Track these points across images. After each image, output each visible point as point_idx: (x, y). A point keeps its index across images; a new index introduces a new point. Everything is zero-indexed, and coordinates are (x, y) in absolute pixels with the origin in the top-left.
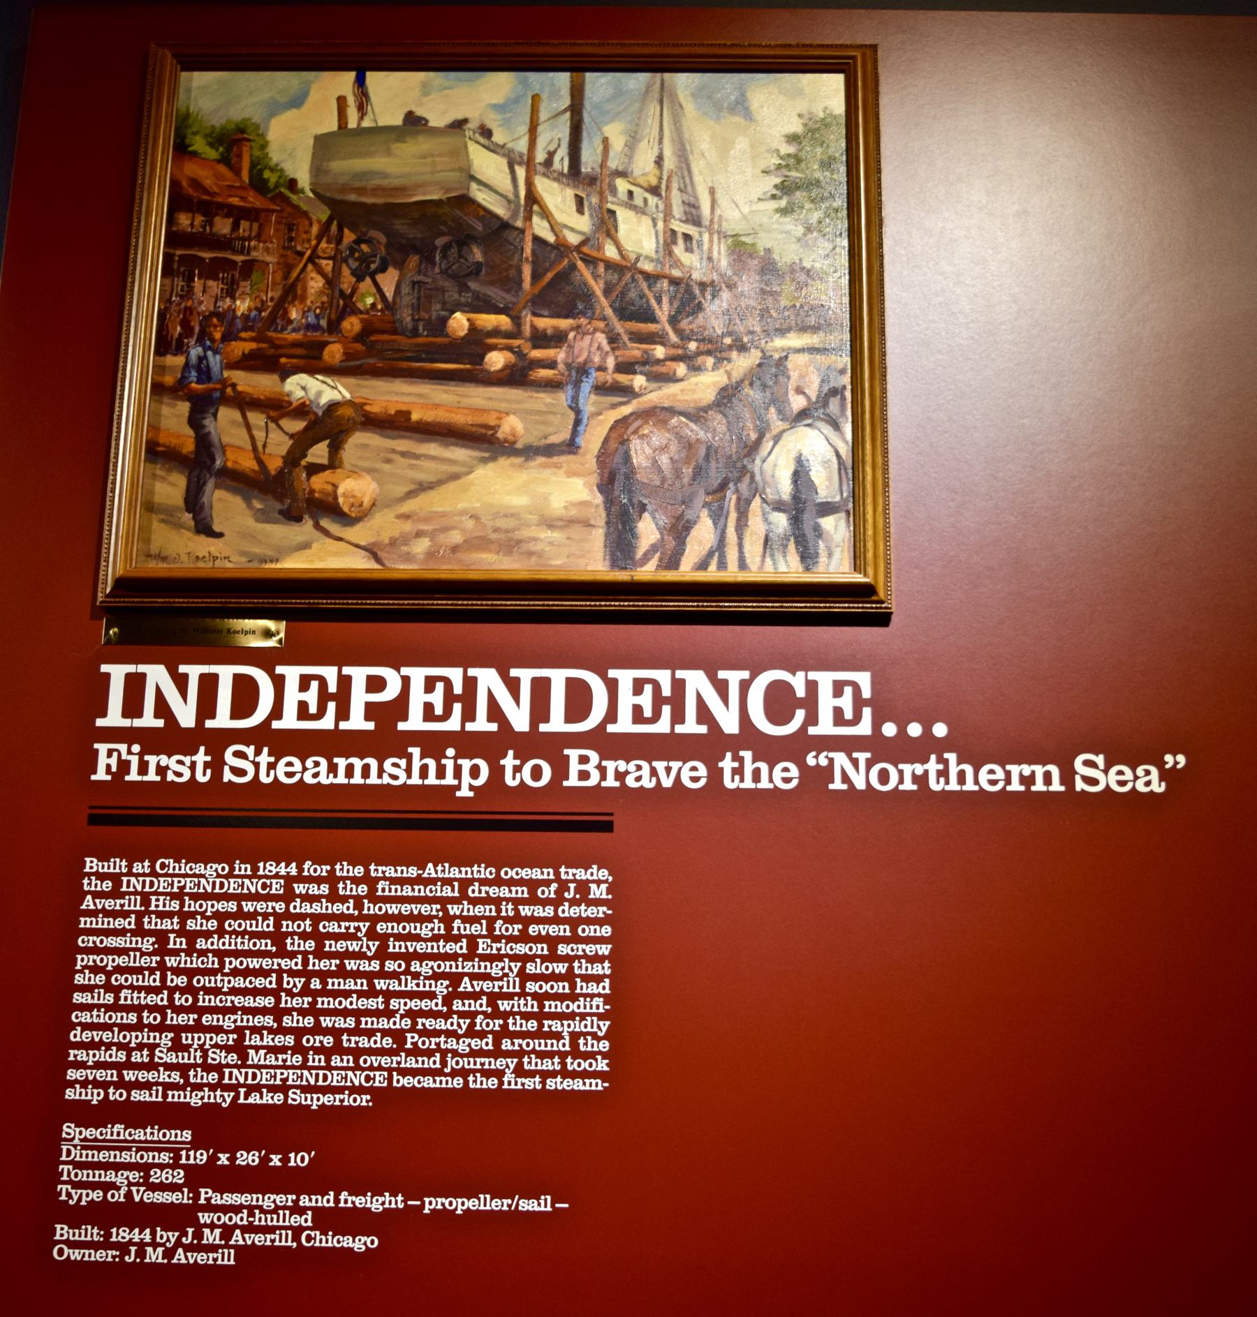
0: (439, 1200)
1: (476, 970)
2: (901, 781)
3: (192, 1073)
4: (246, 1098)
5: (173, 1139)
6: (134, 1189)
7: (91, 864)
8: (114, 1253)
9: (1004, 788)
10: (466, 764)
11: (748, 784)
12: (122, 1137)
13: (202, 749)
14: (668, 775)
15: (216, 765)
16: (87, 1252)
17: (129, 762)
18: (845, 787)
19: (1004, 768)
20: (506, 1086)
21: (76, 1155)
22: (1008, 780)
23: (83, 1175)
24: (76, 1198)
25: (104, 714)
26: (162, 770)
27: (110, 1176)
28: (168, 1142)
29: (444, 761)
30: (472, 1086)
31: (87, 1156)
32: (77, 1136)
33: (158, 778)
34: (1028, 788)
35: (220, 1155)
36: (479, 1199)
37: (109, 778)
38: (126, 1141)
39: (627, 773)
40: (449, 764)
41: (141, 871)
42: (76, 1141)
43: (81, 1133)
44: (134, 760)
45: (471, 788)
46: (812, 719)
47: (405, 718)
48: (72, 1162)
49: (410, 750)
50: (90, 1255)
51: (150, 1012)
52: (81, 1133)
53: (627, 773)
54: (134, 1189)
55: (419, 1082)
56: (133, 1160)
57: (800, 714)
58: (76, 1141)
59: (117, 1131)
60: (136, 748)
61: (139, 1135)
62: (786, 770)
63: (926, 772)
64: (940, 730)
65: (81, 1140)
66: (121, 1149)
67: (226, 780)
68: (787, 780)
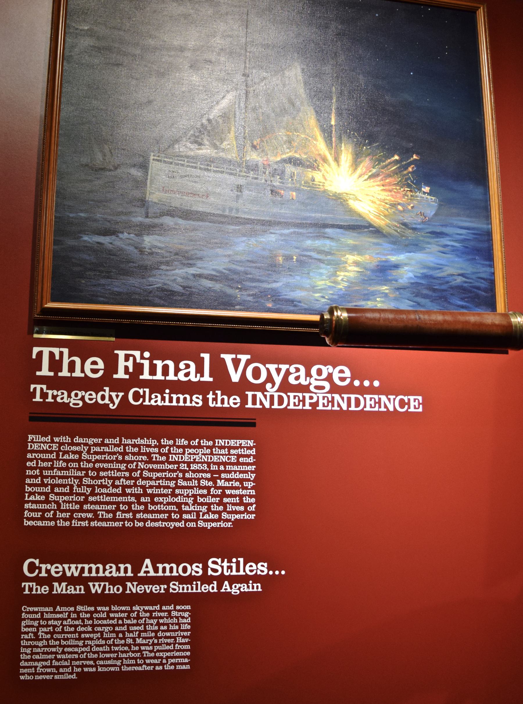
11: (219, 405)
14: (117, 398)
17: (143, 364)
18: (339, 409)
20: (73, 525)
25: (116, 373)
26: (81, 524)
29: (164, 395)
39: (57, 396)
41: (224, 453)
47: (117, 373)
53: (57, 396)
55: (36, 523)
62: (235, 399)
64: (376, 384)
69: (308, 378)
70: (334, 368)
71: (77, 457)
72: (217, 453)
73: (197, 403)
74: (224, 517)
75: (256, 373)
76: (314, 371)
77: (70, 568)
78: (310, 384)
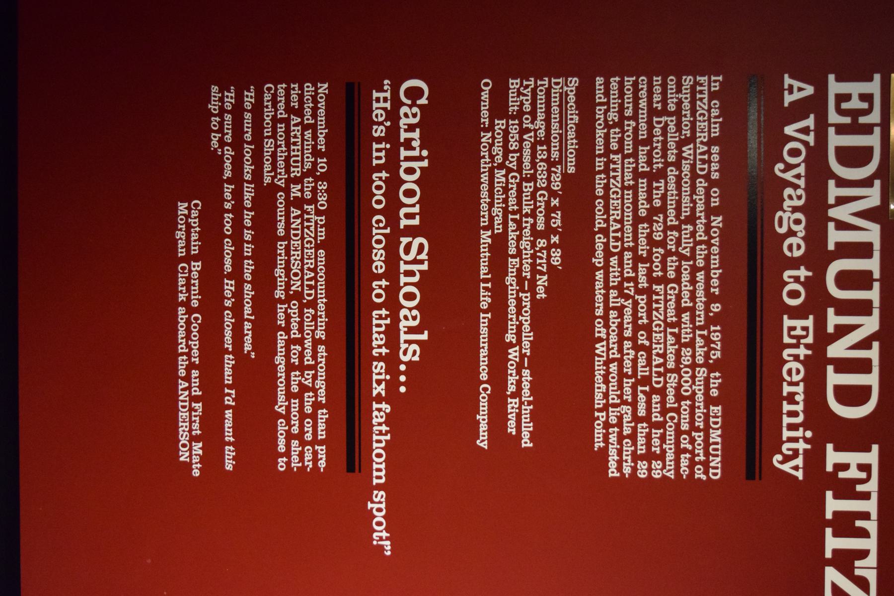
0: (529, 304)
1: (683, 205)
3: (617, 130)
4: (512, 220)
5: (569, 160)
6: (532, 134)
8: (487, 123)
9: (785, 380)
12: (569, 122)
13: (810, 274)
16: (487, 104)
19: (801, 381)
22: (791, 384)
23: (541, 96)
24: (525, 92)
27: (541, 116)
28: (566, 157)
31: (555, 97)
35: (557, 237)
36: (530, 332)
38: (567, 125)
42: (565, 89)
43: (572, 91)
45: (372, 509)
48: (550, 87)
50: (485, 106)
51: (690, 406)
52: (572, 91)
54: (532, 134)
56: (553, 132)
58: (565, 89)
59: (574, 118)
61: (571, 134)
65: (566, 92)
66: (560, 122)
67: (402, 239)
69: (790, 209)
70: (803, 238)
72: (626, 166)
73: (405, 353)
74: (685, 80)
75: (794, 153)
76: (799, 215)
78: (785, 211)
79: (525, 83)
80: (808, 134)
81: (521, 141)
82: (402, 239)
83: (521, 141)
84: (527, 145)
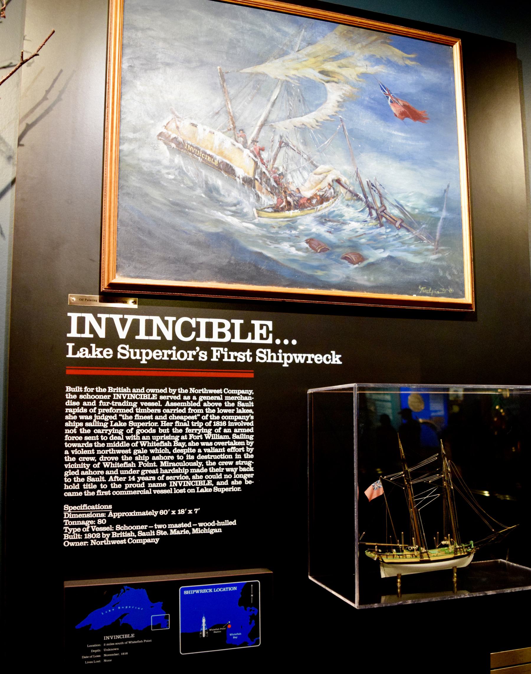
2: (188, 357)
6: (92, 527)
7: (69, 389)
10: (286, 355)
12: (86, 509)
13: (249, 350)
15: (254, 356)
20: (98, 495)
21: (70, 516)
22: (163, 356)
23: (73, 523)
24: (71, 531)
26: (235, 358)
27: (83, 523)
28: (104, 510)
29: (278, 354)
30: (85, 495)
32: (70, 509)
33: (234, 360)
34: (170, 359)
37: (217, 360)
38: (88, 510)
40: (280, 355)
42: (69, 511)
44: (226, 354)
46: (198, 335)
49: (332, 352)
54: (92, 527)
57: (194, 334)
58: (69, 511)
60: (226, 349)
61: (93, 507)
62: (108, 351)
63: (172, 353)
64: (294, 342)
66: (86, 513)
67: (118, 358)
68: (108, 355)
71: (233, 405)
77: (298, 357)
79: (66, 531)
80: (126, 320)
81: (96, 532)
82: (118, 358)
83: (96, 532)
84: (98, 529)
